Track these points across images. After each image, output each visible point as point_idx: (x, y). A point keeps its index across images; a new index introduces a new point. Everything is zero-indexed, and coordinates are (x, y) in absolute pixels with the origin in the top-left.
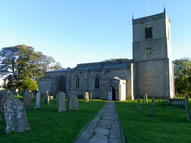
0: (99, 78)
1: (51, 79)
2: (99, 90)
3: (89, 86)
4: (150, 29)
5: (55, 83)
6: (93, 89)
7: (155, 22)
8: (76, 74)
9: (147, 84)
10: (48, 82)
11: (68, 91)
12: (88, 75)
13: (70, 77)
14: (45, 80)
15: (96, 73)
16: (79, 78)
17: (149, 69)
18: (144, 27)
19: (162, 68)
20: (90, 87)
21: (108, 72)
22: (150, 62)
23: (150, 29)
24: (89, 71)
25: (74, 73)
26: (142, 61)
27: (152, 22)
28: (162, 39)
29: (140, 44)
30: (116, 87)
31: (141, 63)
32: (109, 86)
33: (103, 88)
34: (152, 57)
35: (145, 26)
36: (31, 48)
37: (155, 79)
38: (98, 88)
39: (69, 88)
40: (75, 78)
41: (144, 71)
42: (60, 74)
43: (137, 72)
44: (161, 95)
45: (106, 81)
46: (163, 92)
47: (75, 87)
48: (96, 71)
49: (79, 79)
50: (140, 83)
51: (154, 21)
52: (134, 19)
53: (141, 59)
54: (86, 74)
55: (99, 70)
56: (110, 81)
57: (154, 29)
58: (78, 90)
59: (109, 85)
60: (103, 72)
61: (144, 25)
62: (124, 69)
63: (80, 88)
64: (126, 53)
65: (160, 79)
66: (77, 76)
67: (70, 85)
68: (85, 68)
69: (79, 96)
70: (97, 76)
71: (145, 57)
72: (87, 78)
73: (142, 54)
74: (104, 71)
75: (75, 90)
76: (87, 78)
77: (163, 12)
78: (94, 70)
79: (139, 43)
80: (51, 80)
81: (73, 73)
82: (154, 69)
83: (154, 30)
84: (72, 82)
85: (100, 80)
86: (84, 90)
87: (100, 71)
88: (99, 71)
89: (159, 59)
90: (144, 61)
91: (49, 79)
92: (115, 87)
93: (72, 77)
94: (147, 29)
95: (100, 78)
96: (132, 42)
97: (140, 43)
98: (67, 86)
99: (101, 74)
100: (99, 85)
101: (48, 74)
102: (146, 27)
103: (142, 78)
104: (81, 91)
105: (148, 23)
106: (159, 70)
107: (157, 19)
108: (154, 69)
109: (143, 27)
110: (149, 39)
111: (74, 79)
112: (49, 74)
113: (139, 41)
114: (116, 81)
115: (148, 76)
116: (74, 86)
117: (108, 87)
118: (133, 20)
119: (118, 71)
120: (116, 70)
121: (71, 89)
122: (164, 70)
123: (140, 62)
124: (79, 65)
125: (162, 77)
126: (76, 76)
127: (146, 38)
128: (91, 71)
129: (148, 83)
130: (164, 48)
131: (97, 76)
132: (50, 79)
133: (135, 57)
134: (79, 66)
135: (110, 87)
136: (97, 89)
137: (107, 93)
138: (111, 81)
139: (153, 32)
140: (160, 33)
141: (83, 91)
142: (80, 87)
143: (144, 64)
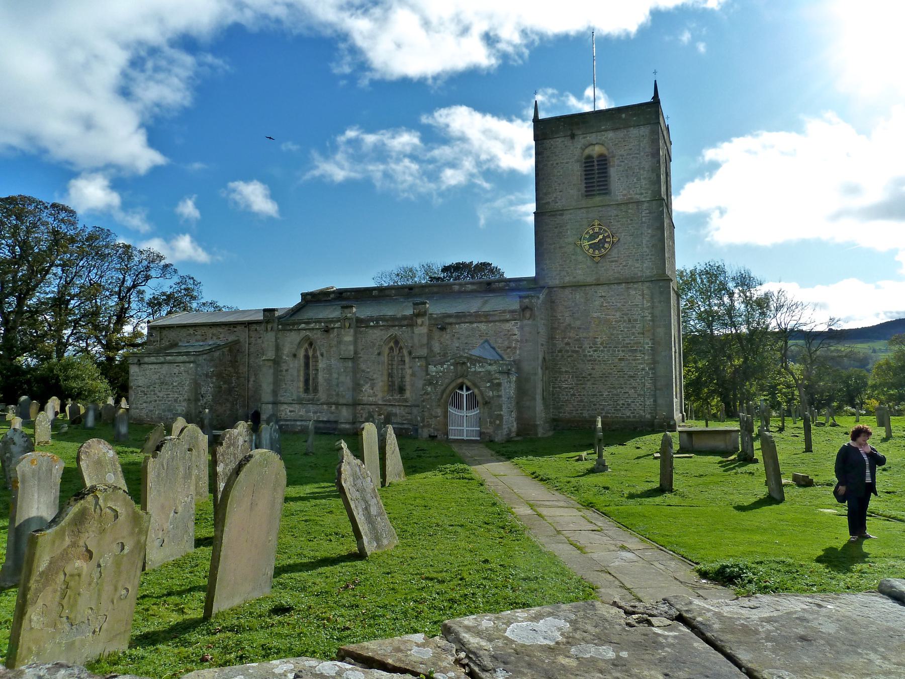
1: (192, 359)
2: (406, 400)
3: (362, 386)
4: (603, 162)
5: (207, 375)
6: (380, 395)
9: (590, 375)
10: (176, 371)
11: (270, 406)
12: (355, 342)
13: (278, 348)
14: (162, 359)
17: (598, 318)
18: (577, 152)
19: (647, 313)
20: (366, 388)
21: (443, 329)
22: (601, 291)
23: (603, 162)
25: (293, 333)
26: (571, 286)
27: (611, 134)
31: (567, 291)
32: (451, 387)
33: (427, 393)
34: (610, 270)
35: (583, 150)
39: (275, 393)
40: (302, 353)
41: (578, 323)
42: (226, 337)
43: (552, 328)
44: (642, 412)
45: (442, 364)
46: (648, 403)
47: (301, 390)
48: (390, 323)
50: (564, 369)
52: (542, 115)
53: (567, 279)
54: (348, 338)
55: (405, 318)
56: (456, 364)
57: (617, 162)
58: (313, 402)
60: (421, 330)
62: (508, 316)
63: (322, 396)
65: (639, 355)
66: (311, 344)
67: (277, 383)
68: (346, 311)
69: (321, 425)
71: (581, 272)
72: (352, 353)
73: (573, 257)
74: (427, 323)
75: (300, 402)
76: (356, 353)
77: (648, 98)
80: (190, 362)
81: (291, 330)
82: (618, 314)
83: (618, 166)
84: (287, 370)
86: (341, 401)
87: (407, 326)
88: (405, 322)
89: (630, 281)
90: (577, 286)
91: (181, 359)
92: (478, 388)
93: (286, 350)
94: (589, 157)
95: (410, 353)
98: (859, 346)
99: (412, 338)
101: (165, 332)
102: (588, 151)
103: (573, 351)
104: (329, 404)
105: (592, 138)
106: (636, 320)
108: (618, 314)
110: (597, 199)
111: (295, 356)
112: (172, 335)
114: (482, 366)
115: (595, 344)
116: (294, 387)
117: (448, 391)
118: (536, 121)
119: (483, 327)
120: (473, 319)
121: (282, 399)
122: (653, 321)
123: (563, 287)
124: (309, 297)
126: (306, 345)
127: (587, 196)
128: (372, 324)
129: (593, 369)
130: (653, 236)
132: (185, 358)
135: (454, 388)
137: (446, 412)
138: (459, 368)
139: (614, 172)
140: (639, 179)
141: (337, 404)
142: (320, 389)
143: (579, 296)
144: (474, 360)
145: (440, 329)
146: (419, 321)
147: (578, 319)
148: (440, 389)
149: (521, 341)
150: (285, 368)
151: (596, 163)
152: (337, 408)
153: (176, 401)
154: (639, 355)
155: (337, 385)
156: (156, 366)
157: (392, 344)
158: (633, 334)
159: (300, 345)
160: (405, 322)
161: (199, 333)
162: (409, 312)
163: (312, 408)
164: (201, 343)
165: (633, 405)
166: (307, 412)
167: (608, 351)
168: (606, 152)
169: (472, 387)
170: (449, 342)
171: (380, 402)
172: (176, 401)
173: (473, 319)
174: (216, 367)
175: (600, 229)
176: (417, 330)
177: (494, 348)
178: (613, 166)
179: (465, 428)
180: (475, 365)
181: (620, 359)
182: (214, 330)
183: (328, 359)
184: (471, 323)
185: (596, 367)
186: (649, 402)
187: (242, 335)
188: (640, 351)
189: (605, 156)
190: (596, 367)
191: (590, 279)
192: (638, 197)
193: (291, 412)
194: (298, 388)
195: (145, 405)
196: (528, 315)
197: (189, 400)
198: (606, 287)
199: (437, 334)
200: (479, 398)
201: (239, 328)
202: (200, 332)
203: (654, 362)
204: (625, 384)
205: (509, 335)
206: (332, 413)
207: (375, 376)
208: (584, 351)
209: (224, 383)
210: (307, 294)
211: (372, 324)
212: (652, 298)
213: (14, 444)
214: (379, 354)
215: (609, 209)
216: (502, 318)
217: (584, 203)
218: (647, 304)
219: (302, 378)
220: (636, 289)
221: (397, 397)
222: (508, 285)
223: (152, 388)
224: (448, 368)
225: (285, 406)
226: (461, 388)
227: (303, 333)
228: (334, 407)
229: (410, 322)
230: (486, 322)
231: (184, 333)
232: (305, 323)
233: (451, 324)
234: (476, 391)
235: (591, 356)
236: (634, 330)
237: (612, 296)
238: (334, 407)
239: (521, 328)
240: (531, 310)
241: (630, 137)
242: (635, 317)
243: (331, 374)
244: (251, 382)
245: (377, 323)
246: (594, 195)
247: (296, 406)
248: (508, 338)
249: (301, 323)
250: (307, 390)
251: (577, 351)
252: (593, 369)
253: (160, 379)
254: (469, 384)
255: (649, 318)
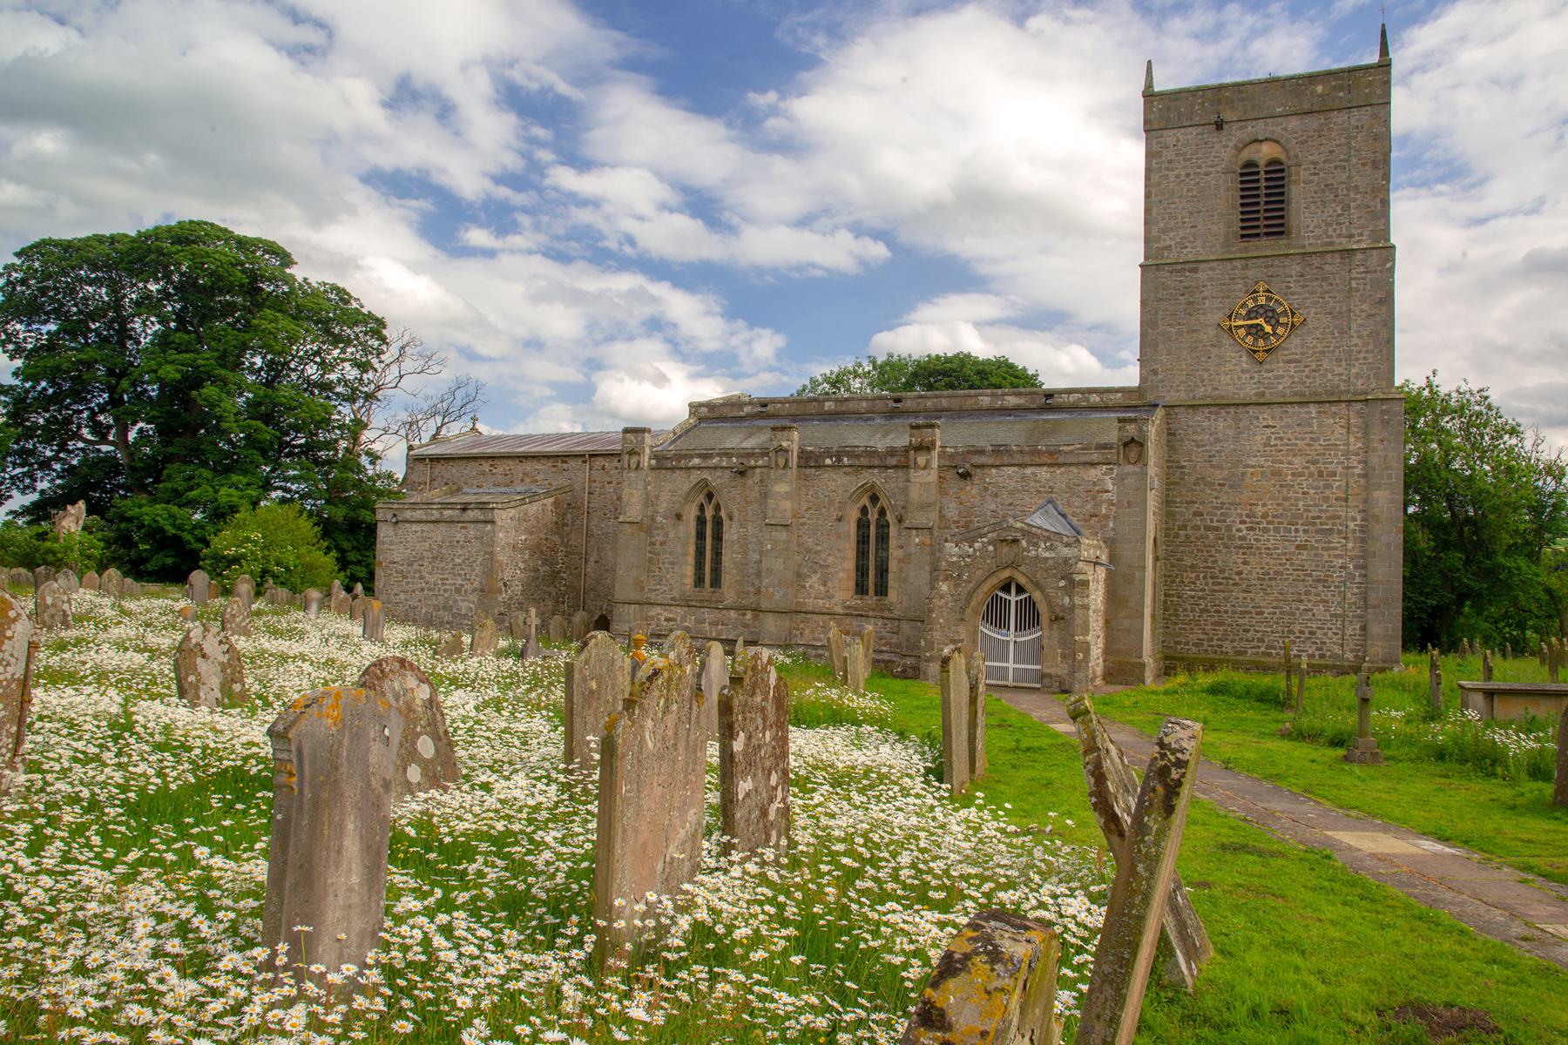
0: (889, 517)
4: (1277, 170)
7: (1313, 122)
8: (696, 476)
9: (1239, 573)
15: (867, 477)
16: (723, 514)
18: (1227, 154)
20: (813, 581)
21: (965, 476)
22: (1265, 416)
23: (1277, 170)
24: (809, 460)
28: (1359, 256)
29: (1199, 275)
30: (1051, 592)
35: (1240, 150)
36: (273, 249)
37: (1302, 537)
38: (882, 590)
40: (691, 513)
44: (1337, 650)
47: (689, 581)
48: (864, 461)
49: (726, 522)
51: (1308, 119)
52: (1156, 89)
55: (892, 452)
57: (1303, 175)
58: (705, 604)
59: (1049, 603)
61: (1235, 135)
62: (1095, 457)
63: (729, 593)
64: (1409, 373)
65: (1336, 540)
66: (710, 496)
70: (874, 499)
74: (935, 464)
75: (687, 603)
77: (1373, 58)
78: (849, 454)
79: (1194, 265)
81: (672, 469)
82: (1298, 462)
85: (893, 531)
87: (895, 467)
88: (892, 461)
94: (1250, 164)
96: (1142, 260)
97: (1195, 270)
100: (883, 571)
102: (1247, 155)
103: (1208, 528)
104: (742, 609)
106: (1334, 474)
107: (1324, 109)
108: (1298, 462)
109: (1224, 152)
110: (1266, 246)
111: (679, 517)
113: (1189, 254)
114: (1051, 548)
118: (1149, 95)
119: (1044, 473)
125: (1351, 525)
126: (701, 498)
127: (1243, 236)
128: (828, 461)
131: (874, 499)
133: (1155, 372)
134: (701, 420)
136: (871, 599)
139: (1299, 196)
140: (1346, 208)
142: (726, 580)
143: (1222, 424)
144: (1031, 535)
145: (961, 475)
146: (921, 460)
147: (1220, 467)
148: (964, 590)
149: (1119, 504)
150: (661, 538)
151: (1263, 176)
152: (755, 617)
153: (458, 590)
154: (1336, 540)
155: (758, 574)
156: (426, 527)
157: (865, 501)
158: (1326, 499)
159: (688, 497)
160: (892, 461)
161: (500, 470)
162: (902, 440)
163: (708, 615)
164: (503, 489)
165: (1319, 634)
166: (700, 621)
167: (1277, 530)
168: (1282, 157)
169: (1028, 587)
170: (976, 501)
171: (838, 610)
172: (458, 590)
173: (1027, 459)
174: (531, 533)
175: (1269, 299)
176: (917, 477)
177: (1064, 516)
178: (1297, 182)
179: (1011, 665)
180: (1036, 545)
181: (1298, 547)
182: (529, 466)
183: (742, 526)
184: (1022, 466)
185: (1251, 559)
186: (1353, 629)
187: (579, 474)
188: (1340, 532)
189: (1281, 163)
190: (1251, 559)
191: (1249, 391)
192: (1345, 240)
193: (667, 620)
194: (683, 576)
195: (402, 596)
196: (1133, 455)
197: (482, 590)
198: (1277, 410)
199: (954, 484)
200: (1042, 608)
201: (573, 463)
202: (501, 468)
203: (1365, 555)
204: (1307, 593)
205: (1095, 492)
206: (745, 626)
207: (830, 560)
208: (1229, 528)
209: (544, 564)
210: (701, 405)
211: (828, 461)
212: (1366, 434)
213: (204, 656)
214: (839, 520)
215: (1287, 262)
216: (1083, 459)
217: (1238, 248)
218: (1356, 445)
219: (691, 559)
220: (1334, 415)
221: (871, 599)
222: (1088, 400)
223: (416, 566)
224: (983, 549)
225: (658, 609)
226: (1006, 588)
227: (696, 476)
228: (749, 615)
229: (901, 461)
230: (1050, 465)
231: (472, 469)
232: (699, 456)
233: (982, 466)
234: (1037, 596)
235: (1243, 538)
236: (1328, 493)
237: (1287, 426)
238: (749, 615)
239: (1119, 480)
240: (1141, 445)
241: (1330, 130)
242: (1332, 467)
243: (745, 553)
244: (591, 564)
245: (839, 460)
246: (1257, 235)
247: (679, 610)
248: (1094, 498)
249: (692, 457)
250: (699, 581)
251: (1217, 529)
252: (1245, 563)
253: (430, 550)
254: (1022, 580)
255: (1357, 471)
